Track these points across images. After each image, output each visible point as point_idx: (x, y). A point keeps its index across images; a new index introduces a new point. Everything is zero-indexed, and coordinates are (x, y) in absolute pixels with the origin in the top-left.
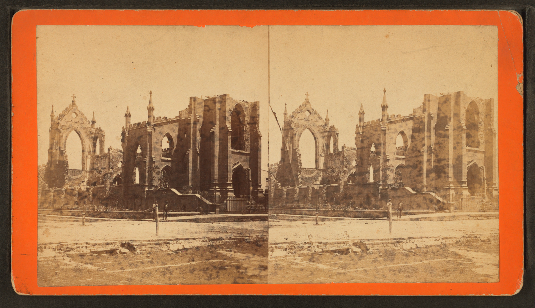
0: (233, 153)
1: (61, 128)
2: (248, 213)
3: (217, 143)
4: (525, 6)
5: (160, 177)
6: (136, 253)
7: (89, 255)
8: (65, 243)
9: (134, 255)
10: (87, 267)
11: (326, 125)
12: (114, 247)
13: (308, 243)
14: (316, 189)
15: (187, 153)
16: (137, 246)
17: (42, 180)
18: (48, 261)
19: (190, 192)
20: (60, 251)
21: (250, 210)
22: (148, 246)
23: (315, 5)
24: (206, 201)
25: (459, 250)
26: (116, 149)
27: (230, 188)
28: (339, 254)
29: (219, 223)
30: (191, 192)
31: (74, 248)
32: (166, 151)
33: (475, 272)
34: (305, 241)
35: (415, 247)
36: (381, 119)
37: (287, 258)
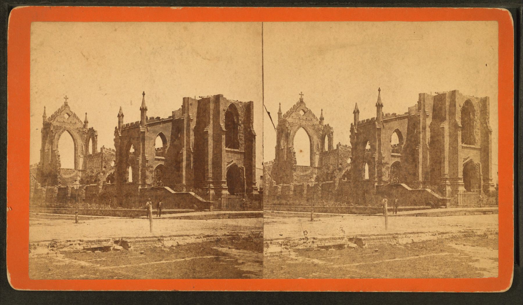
0: (227, 151)
1: (53, 129)
3: (211, 142)
4: (520, 5)
5: (153, 175)
7: (82, 252)
8: (58, 240)
9: (362, 250)
10: (81, 264)
12: (108, 244)
13: (303, 239)
15: (181, 152)
16: (131, 242)
17: (269, 177)
18: (42, 258)
19: (421, 188)
21: (243, 207)
22: (376, 241)
23: (311, 3)
24: (200, 199)
25: (456, 244)
27: (225, 186)
28: (100, 252)
29: (213, 220)
30: (185, 190)
31: (68, 245)
32: (396, 147)
33: (472, 266)
34: (300, 237)
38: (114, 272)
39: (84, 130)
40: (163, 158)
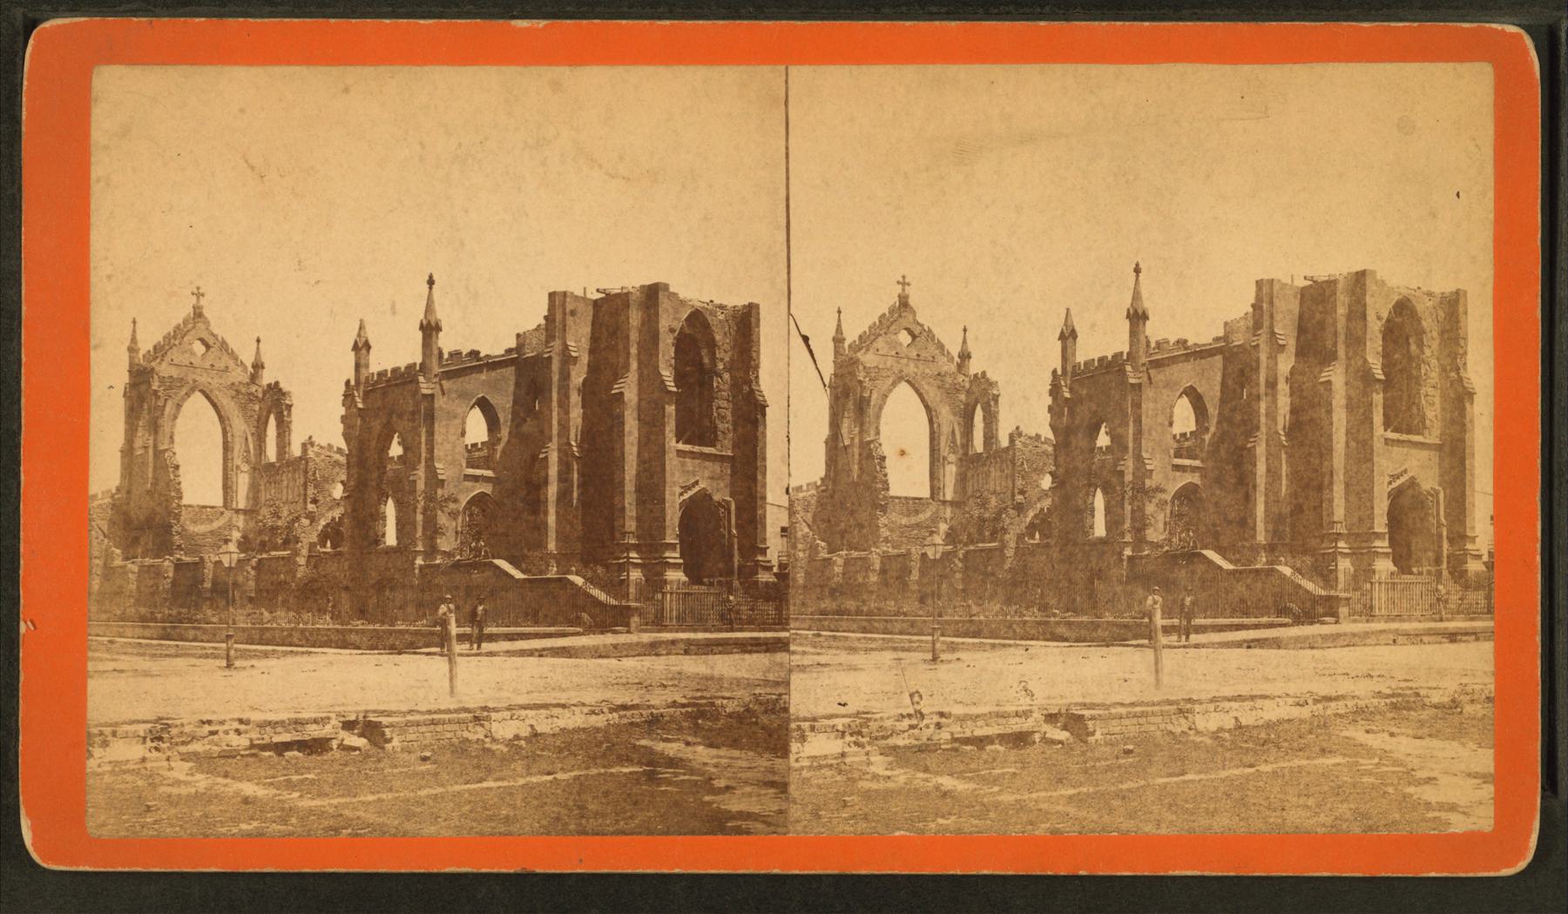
0: (680, 453)
1: (160, 387)
2: (727, 631)
3: (631, 424)
4: (1560, 14)
5: (460, 525)
6: (1094, 742)
7: (247, 755)
11: (254, 378)
13: (909, 716)
14: (227, 565)
15: (542, 456)
16: (393, 726)
19: (1261, 562)
20: (860, 738)
21: (729, 620)
23: (934, 9)
24: (601, 596)
25: (1368, 732)
26: (324, 444)
27: (674, 556)
28: (301, 755)
29: (640, 658)
30: (555, 569)
31: (203, 735)
32: (1187, 440)
35: (1232, 727)
36: (1128, 354)
37: (148, 765)
38: (341, 815)
39: (253, 389)
40: (489, 473)
